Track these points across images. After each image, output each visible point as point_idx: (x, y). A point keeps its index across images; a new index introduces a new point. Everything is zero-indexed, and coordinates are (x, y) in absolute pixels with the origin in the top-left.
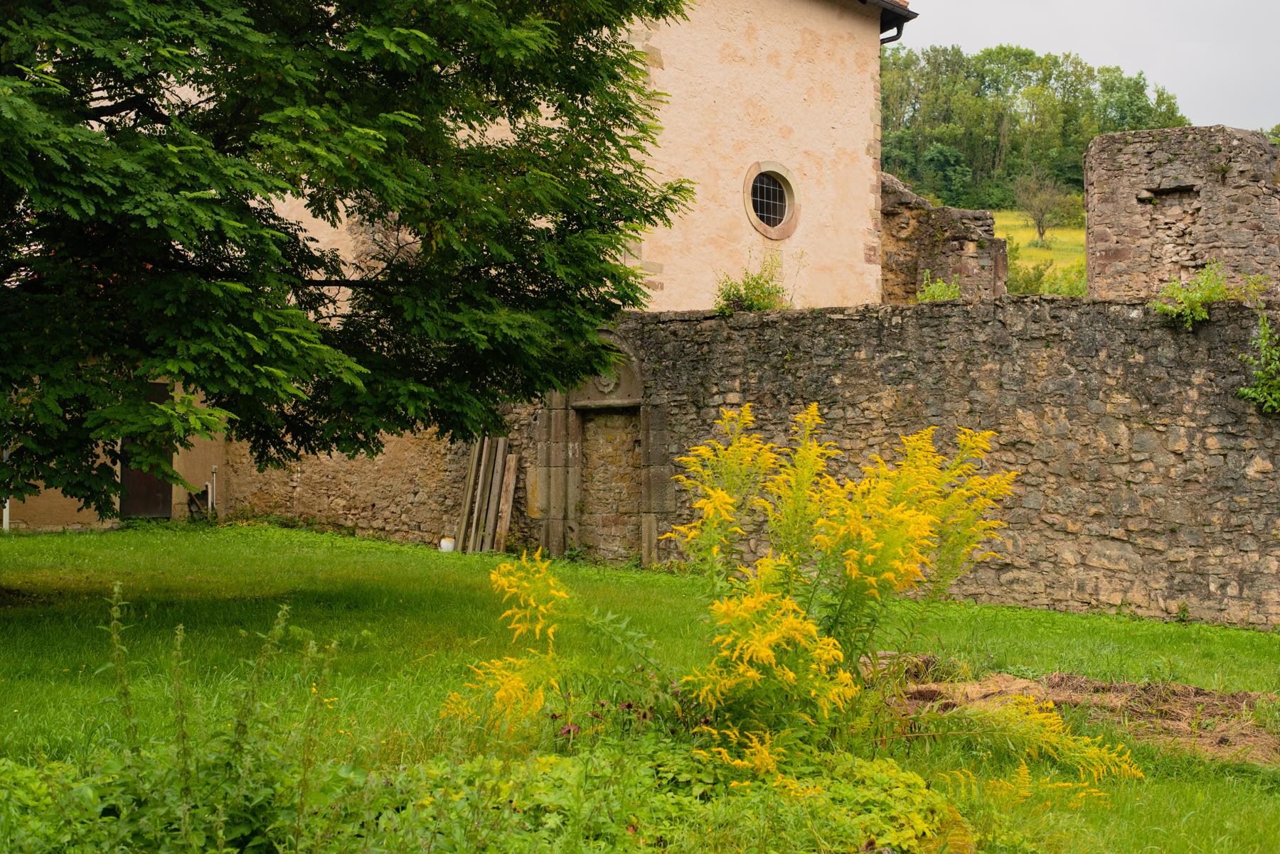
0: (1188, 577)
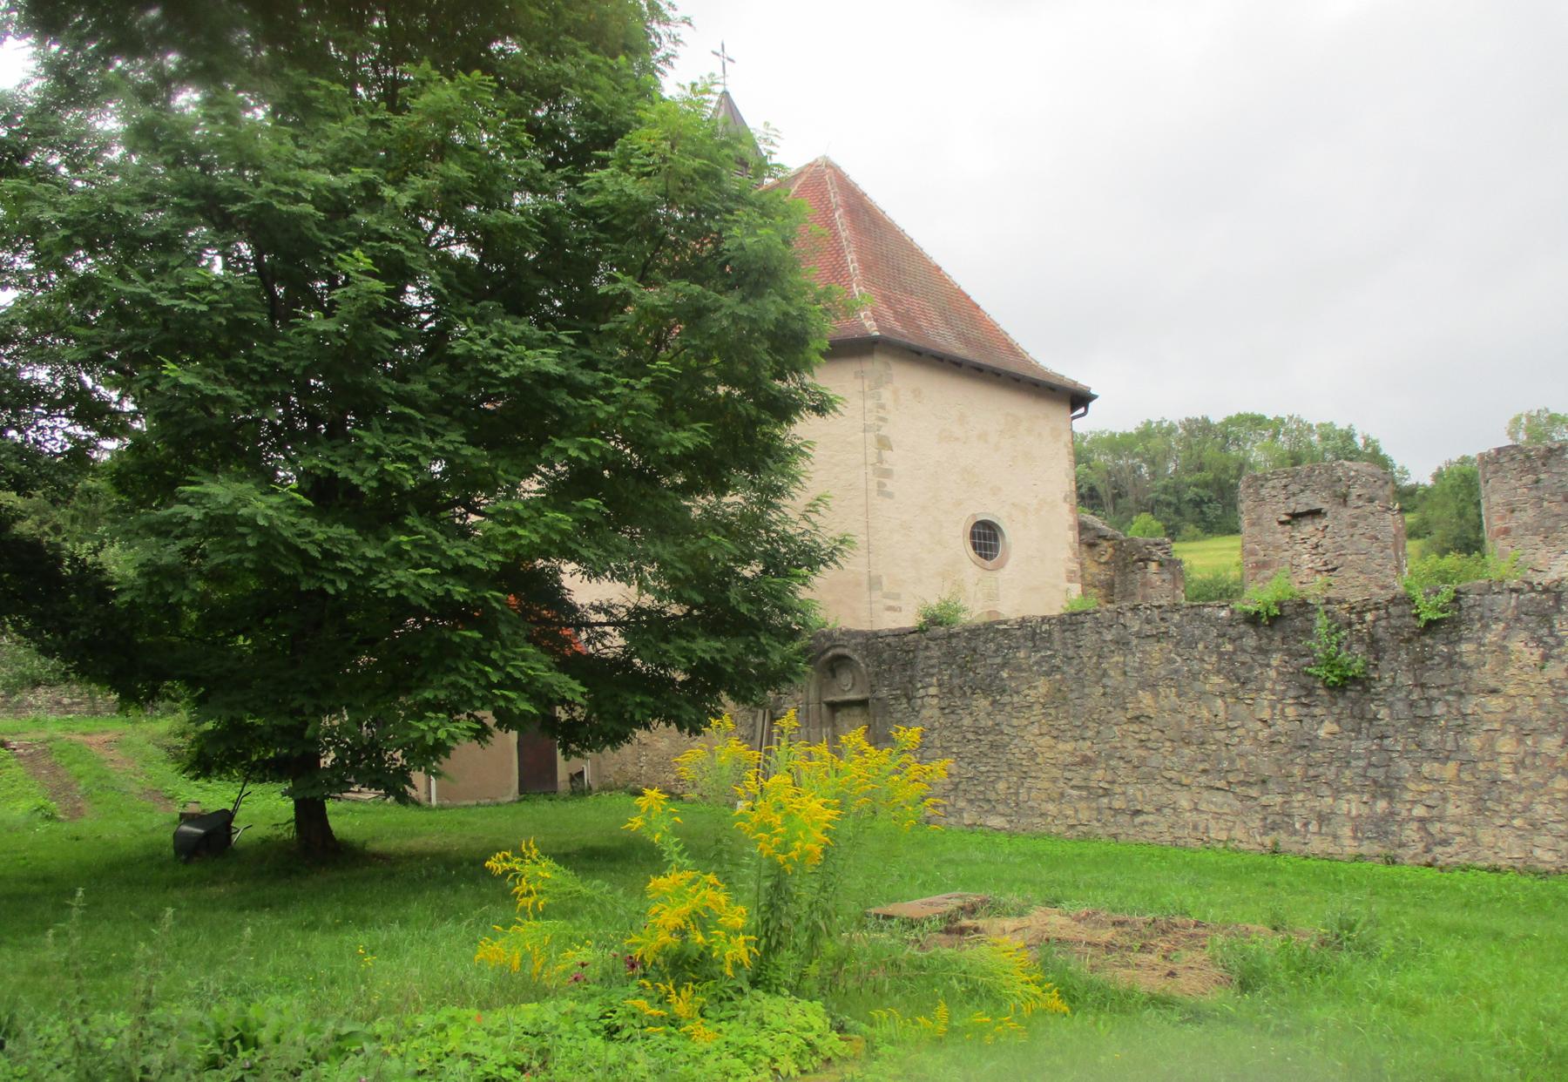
0: (1278, 819)
